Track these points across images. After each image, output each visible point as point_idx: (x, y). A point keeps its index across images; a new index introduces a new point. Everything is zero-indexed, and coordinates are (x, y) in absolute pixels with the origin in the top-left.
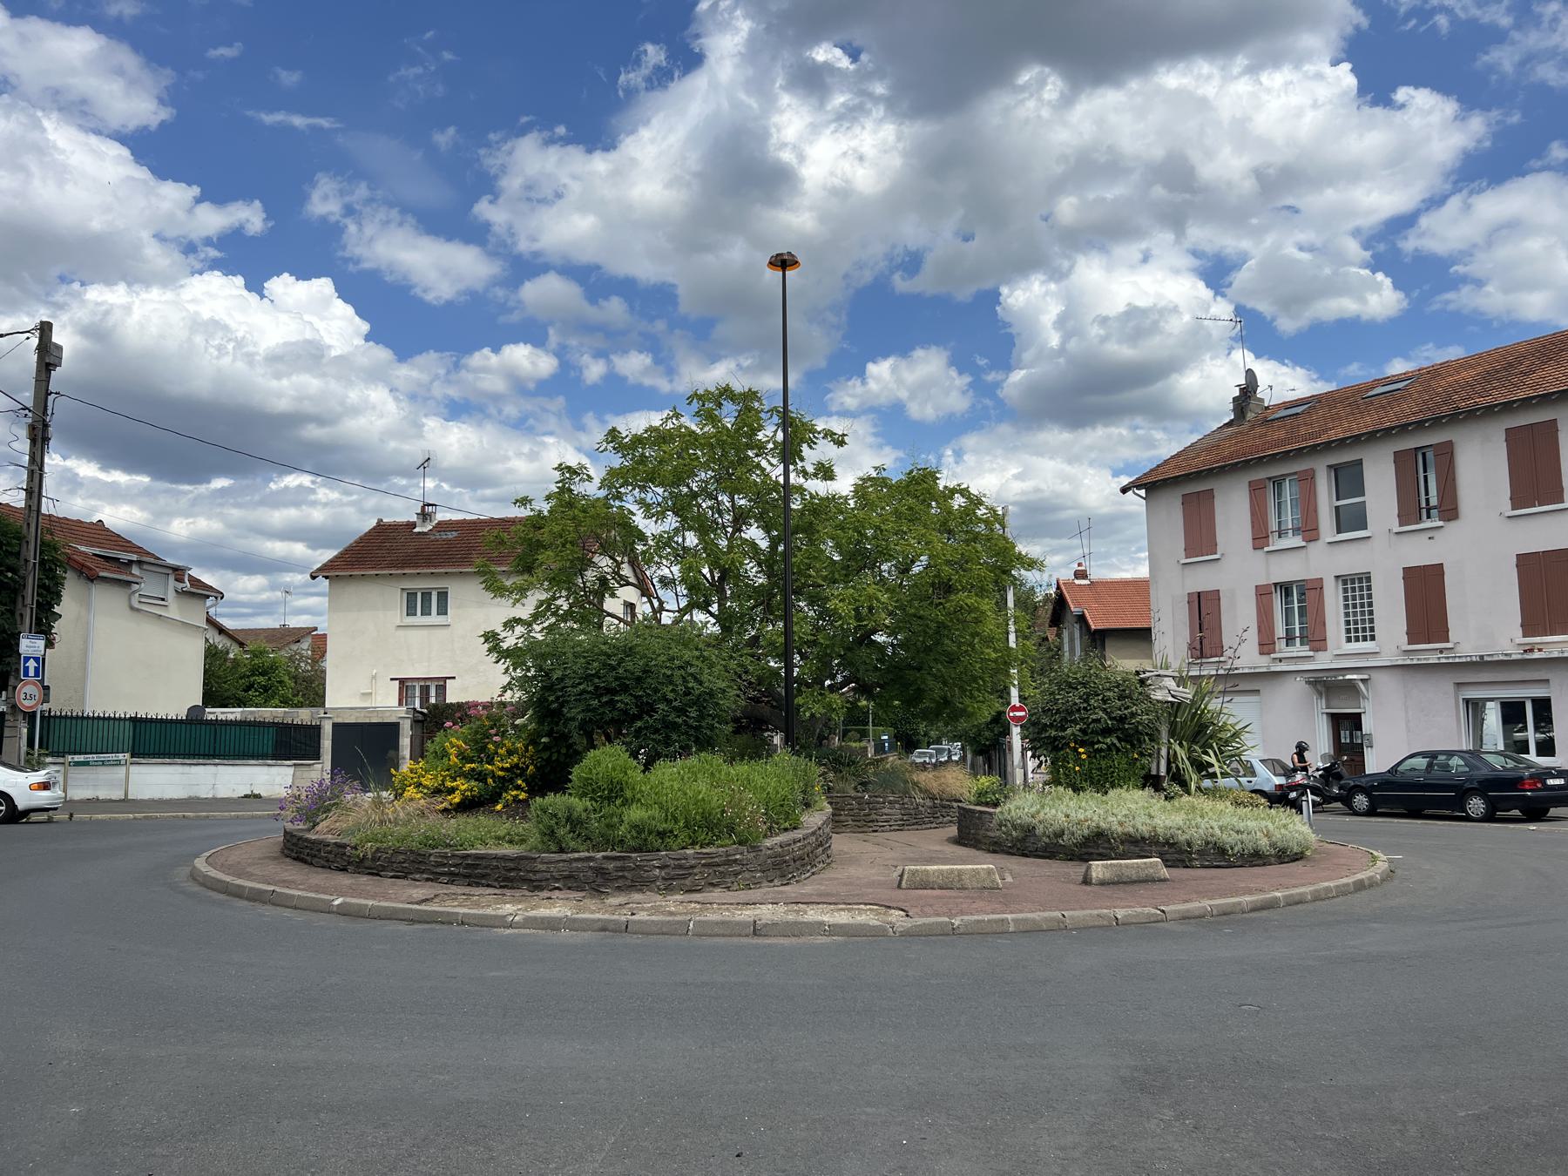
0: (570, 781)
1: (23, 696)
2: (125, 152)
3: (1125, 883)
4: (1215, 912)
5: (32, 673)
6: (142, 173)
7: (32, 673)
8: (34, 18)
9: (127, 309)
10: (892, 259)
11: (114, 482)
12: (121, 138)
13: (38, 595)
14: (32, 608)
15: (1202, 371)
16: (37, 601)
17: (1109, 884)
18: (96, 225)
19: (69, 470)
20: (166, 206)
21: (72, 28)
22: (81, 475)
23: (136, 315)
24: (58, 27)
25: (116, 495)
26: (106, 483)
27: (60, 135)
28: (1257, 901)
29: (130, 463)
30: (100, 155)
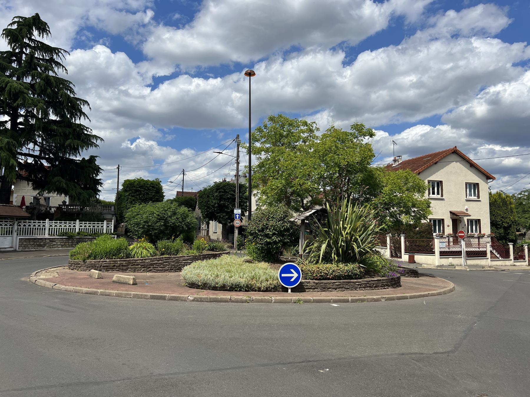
0: (193, 244)
1: (235, 223)
2: (499, 41)
3: (119, 283)
4: (73, 291)
5: (238, 218)
6: (507, 44)
7: (238, 218)
8: (463, 10)
9: (505, 90)
10: (200, 69)
11: (507, 150)
12: (496, 37)
13: (239, 199)
14: (237, 203)
15: (140, 93)
16: (239, 201)
17: (115, 282)
18: (491, 68)
19: (491, 149)
20: (514, 53)
21: (476, 7)
22: (496, 150)
23: (508, 92)
24: (472, 9)
25: (508, 155)
26: (504, 151)
27: (477, 43)
28: (89, 291)
29: (511, 143)
30: (491, 44)
